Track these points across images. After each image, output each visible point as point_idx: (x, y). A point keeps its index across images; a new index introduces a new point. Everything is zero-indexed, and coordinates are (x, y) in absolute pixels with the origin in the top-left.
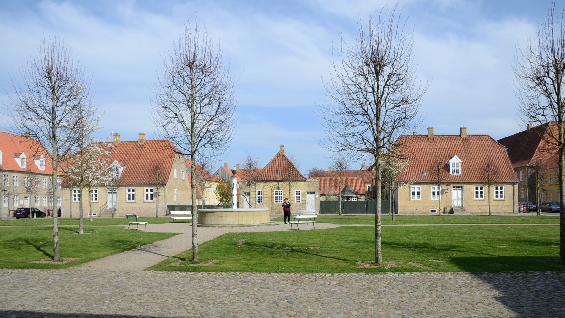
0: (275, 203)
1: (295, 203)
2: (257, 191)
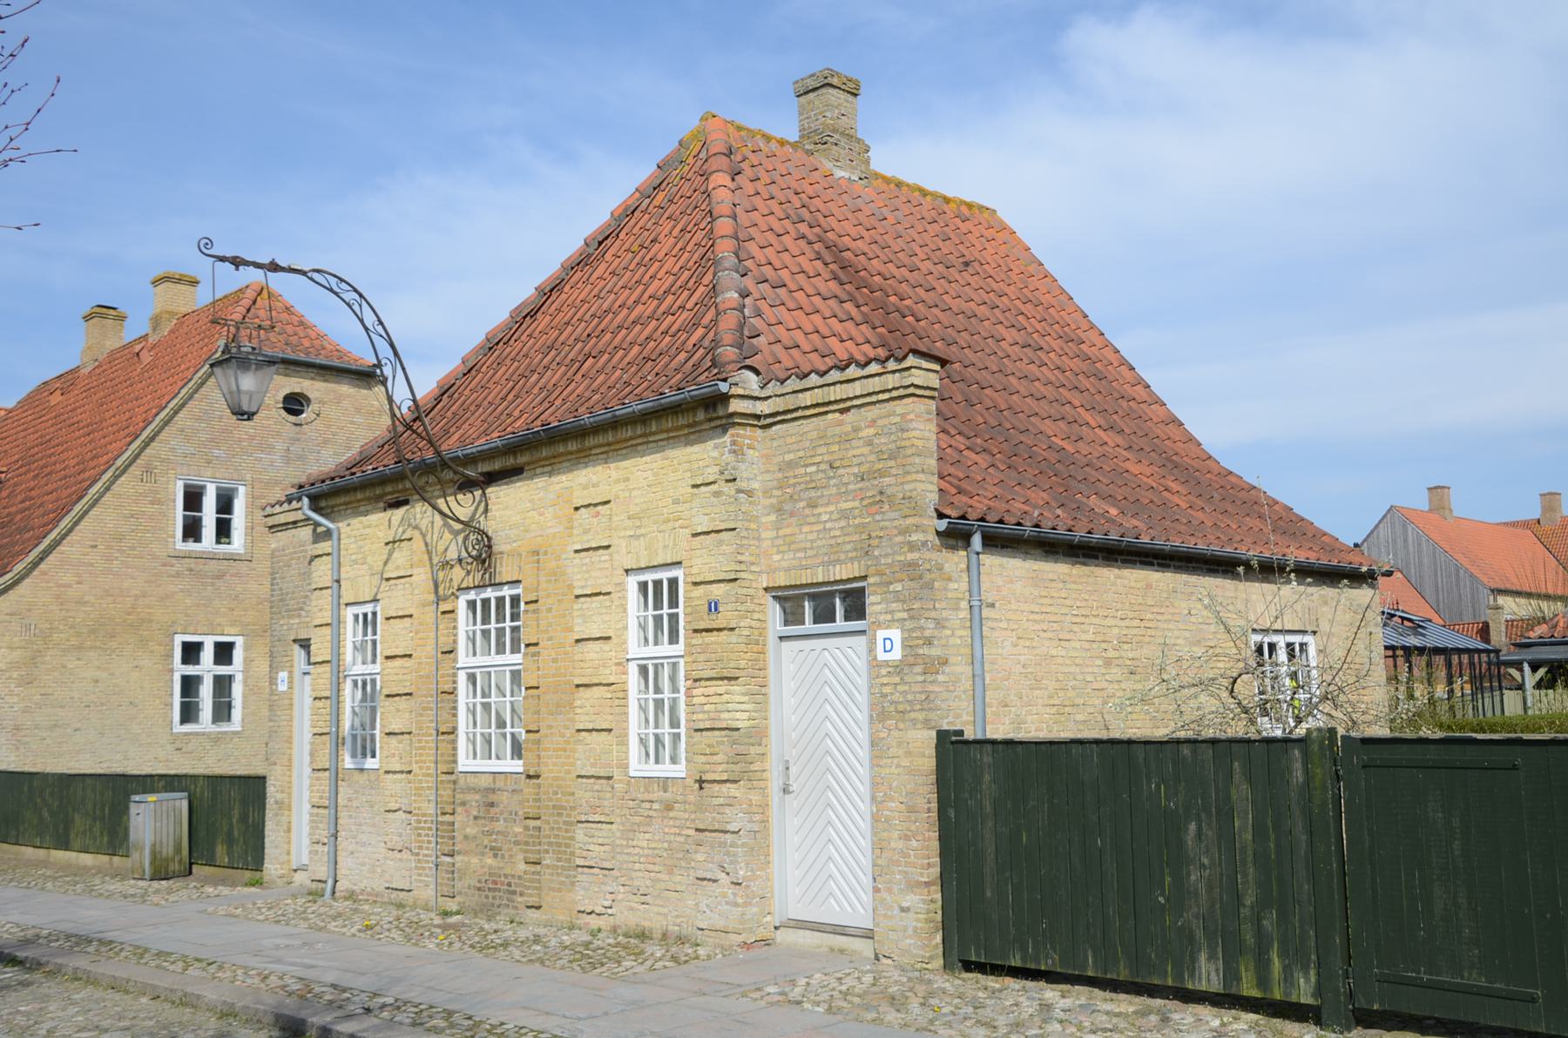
0: (465, 763)
1: (638, 766)
2: (349, 613)
